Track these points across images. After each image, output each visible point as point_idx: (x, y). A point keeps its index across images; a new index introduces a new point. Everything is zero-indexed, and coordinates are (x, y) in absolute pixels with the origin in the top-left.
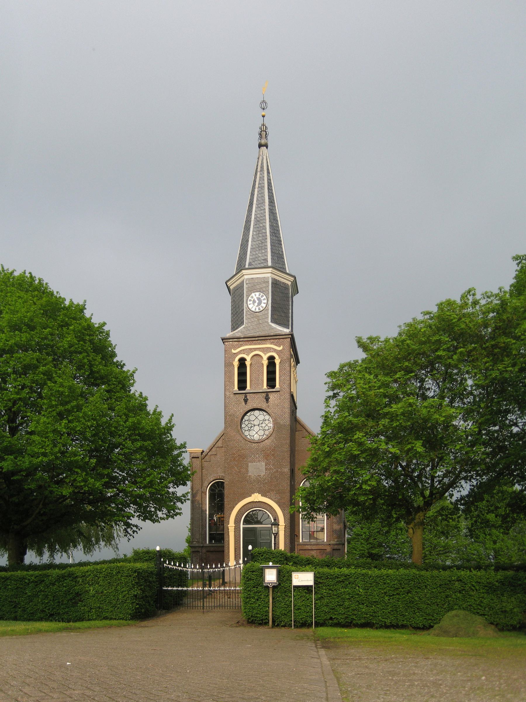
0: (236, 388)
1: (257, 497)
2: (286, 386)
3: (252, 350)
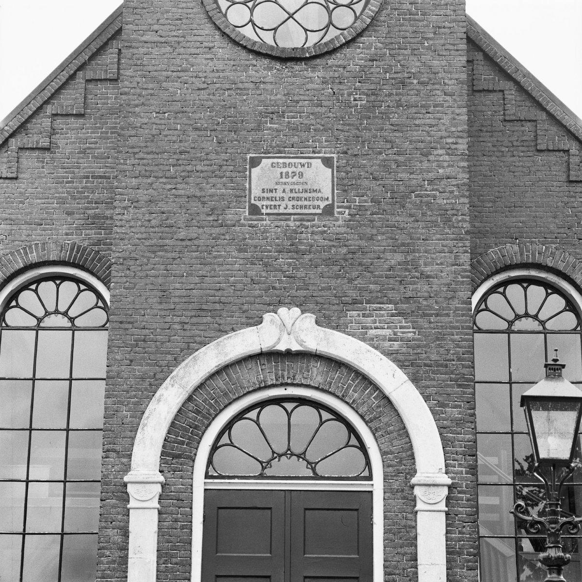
1: (290, 328)
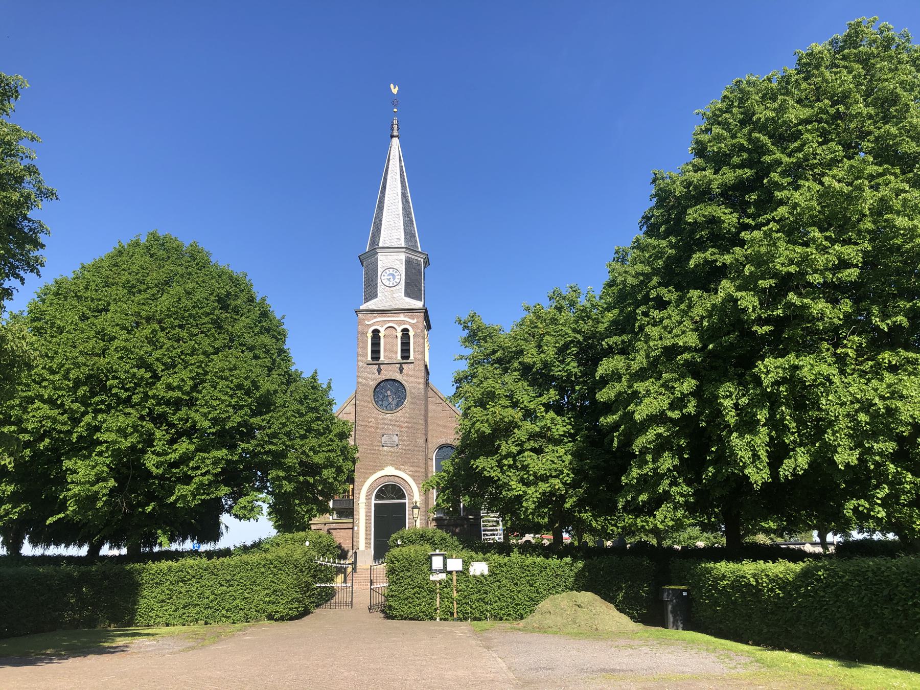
0: (399, 357)
2: (420, 358)
3: (404, 322)
